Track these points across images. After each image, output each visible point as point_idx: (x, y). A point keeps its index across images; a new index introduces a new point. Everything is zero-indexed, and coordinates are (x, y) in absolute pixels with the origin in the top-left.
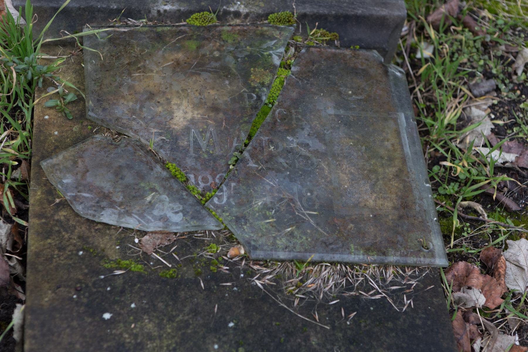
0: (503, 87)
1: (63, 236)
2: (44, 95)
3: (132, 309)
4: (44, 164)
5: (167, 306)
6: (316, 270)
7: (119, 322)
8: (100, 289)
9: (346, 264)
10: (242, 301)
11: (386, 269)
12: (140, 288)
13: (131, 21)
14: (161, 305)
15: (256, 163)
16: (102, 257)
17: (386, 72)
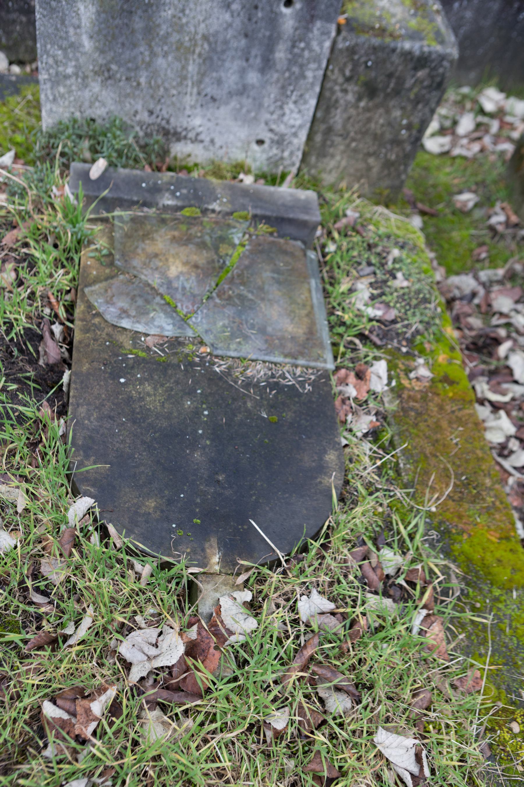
0: (378, 272)
2: (87, 249)
4: (86, 290)
5: (160, 377)
9: (272, 363)
13: (146, 209)
14: (156, 377)
15: (221, 299)
16: (121, 347)
17: (305, 255)
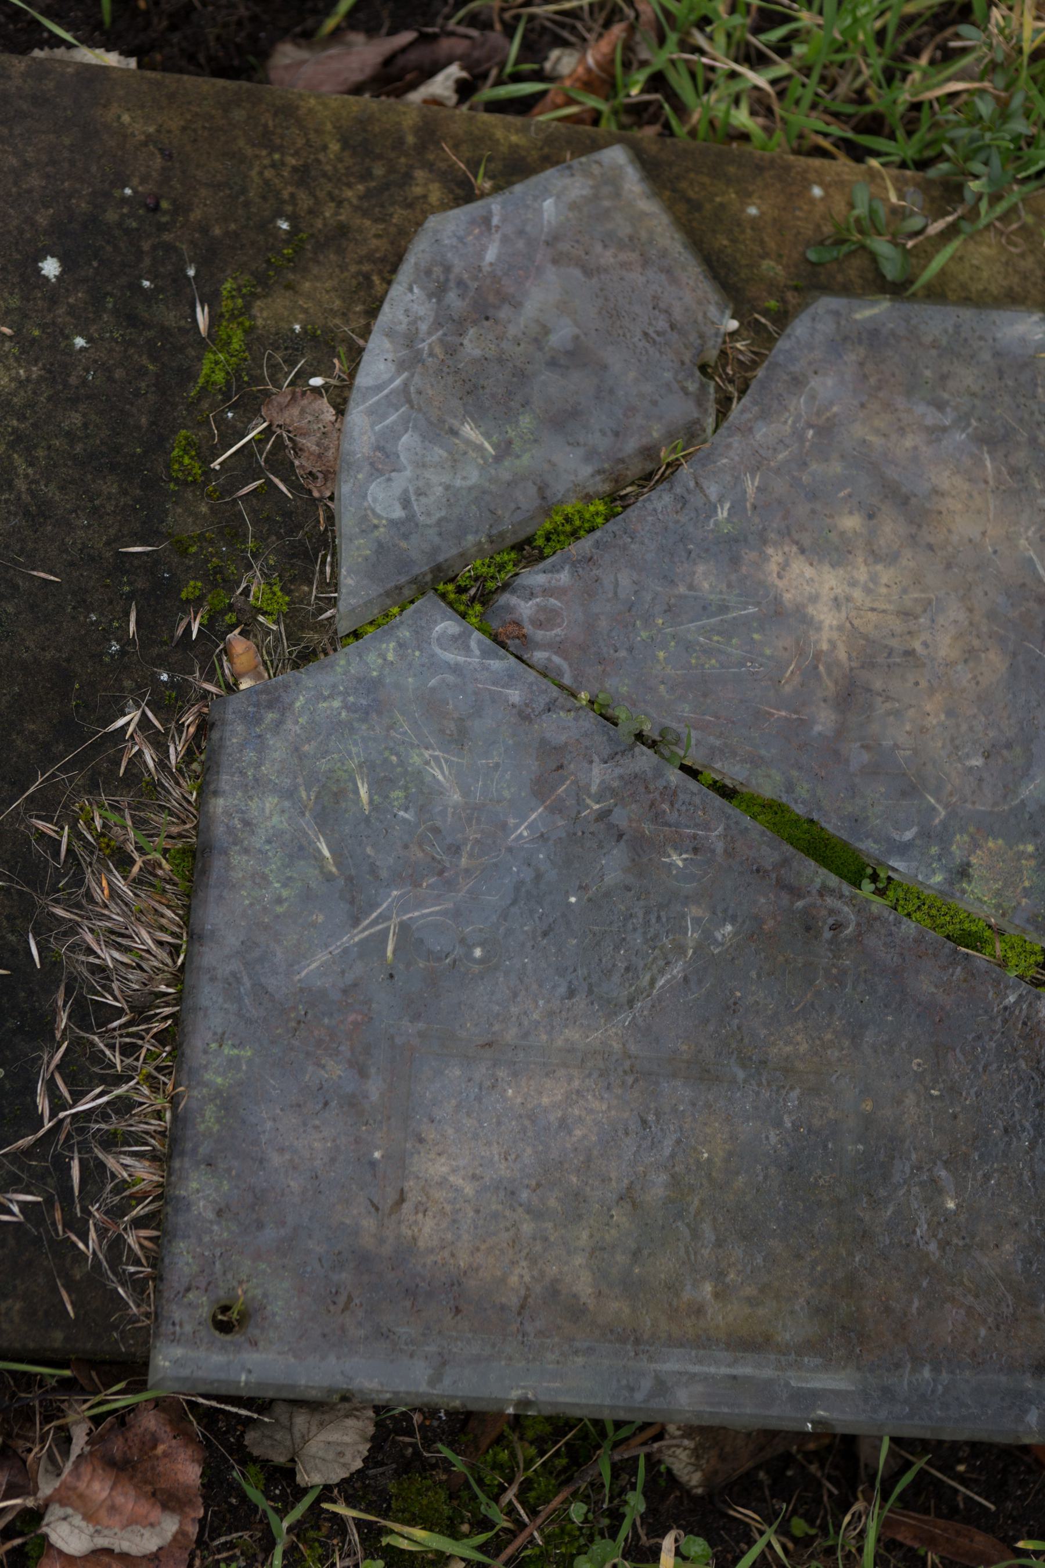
1: (349, 185)
3: (68, 338)
6: (162, 916)
7: (26, 298)
8: (147, 262)
10: (68, 660)
11: (154, 1157)
12: (142, 372)
